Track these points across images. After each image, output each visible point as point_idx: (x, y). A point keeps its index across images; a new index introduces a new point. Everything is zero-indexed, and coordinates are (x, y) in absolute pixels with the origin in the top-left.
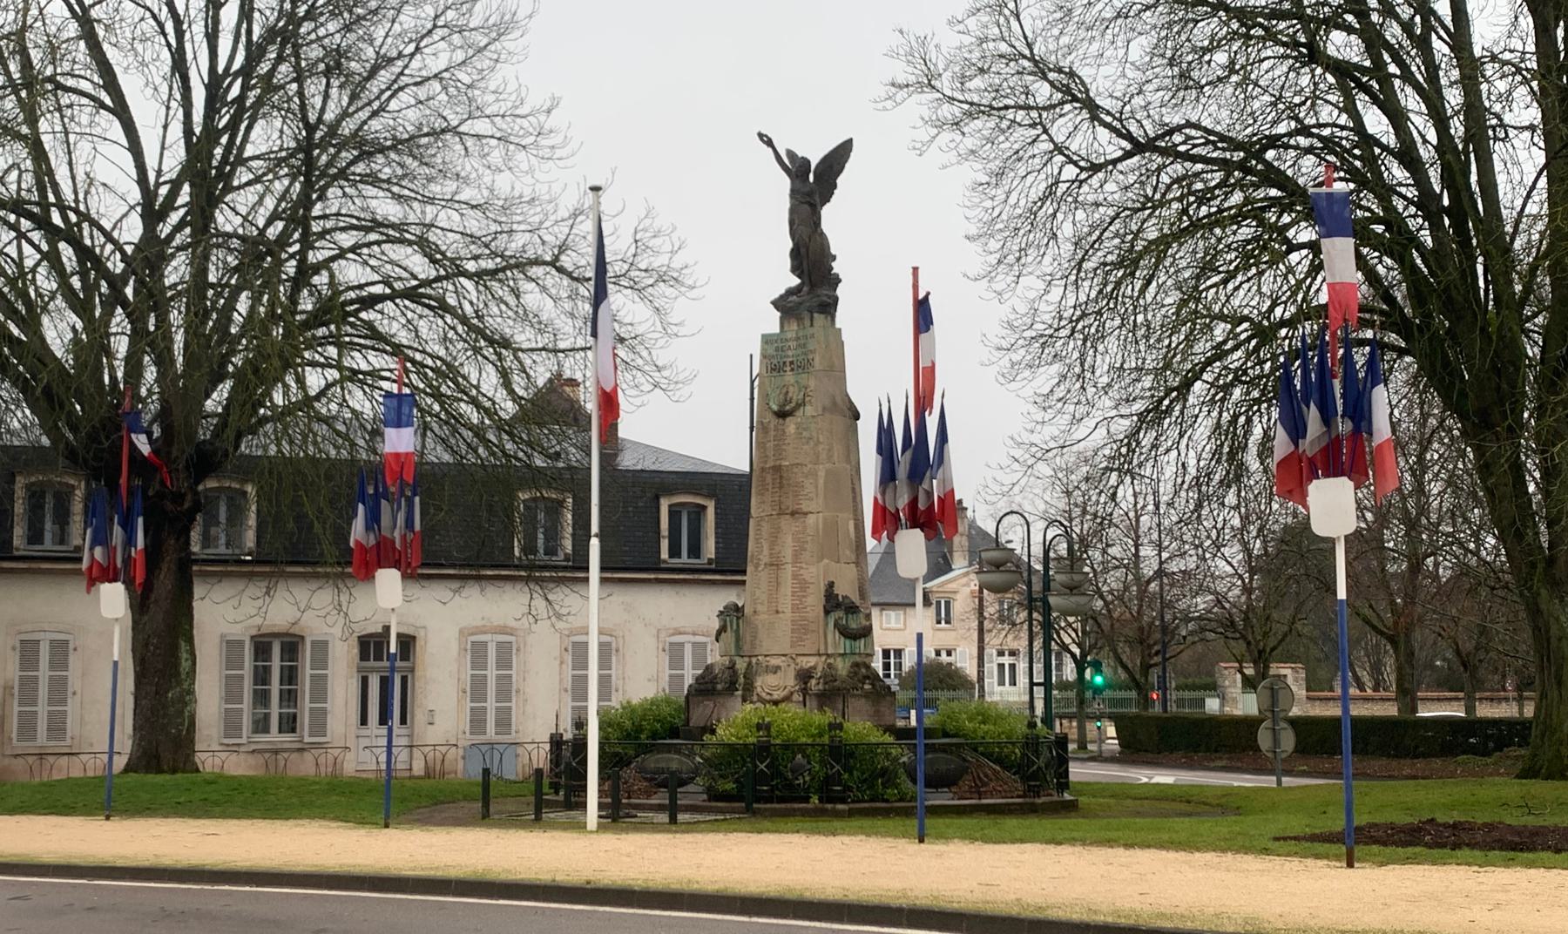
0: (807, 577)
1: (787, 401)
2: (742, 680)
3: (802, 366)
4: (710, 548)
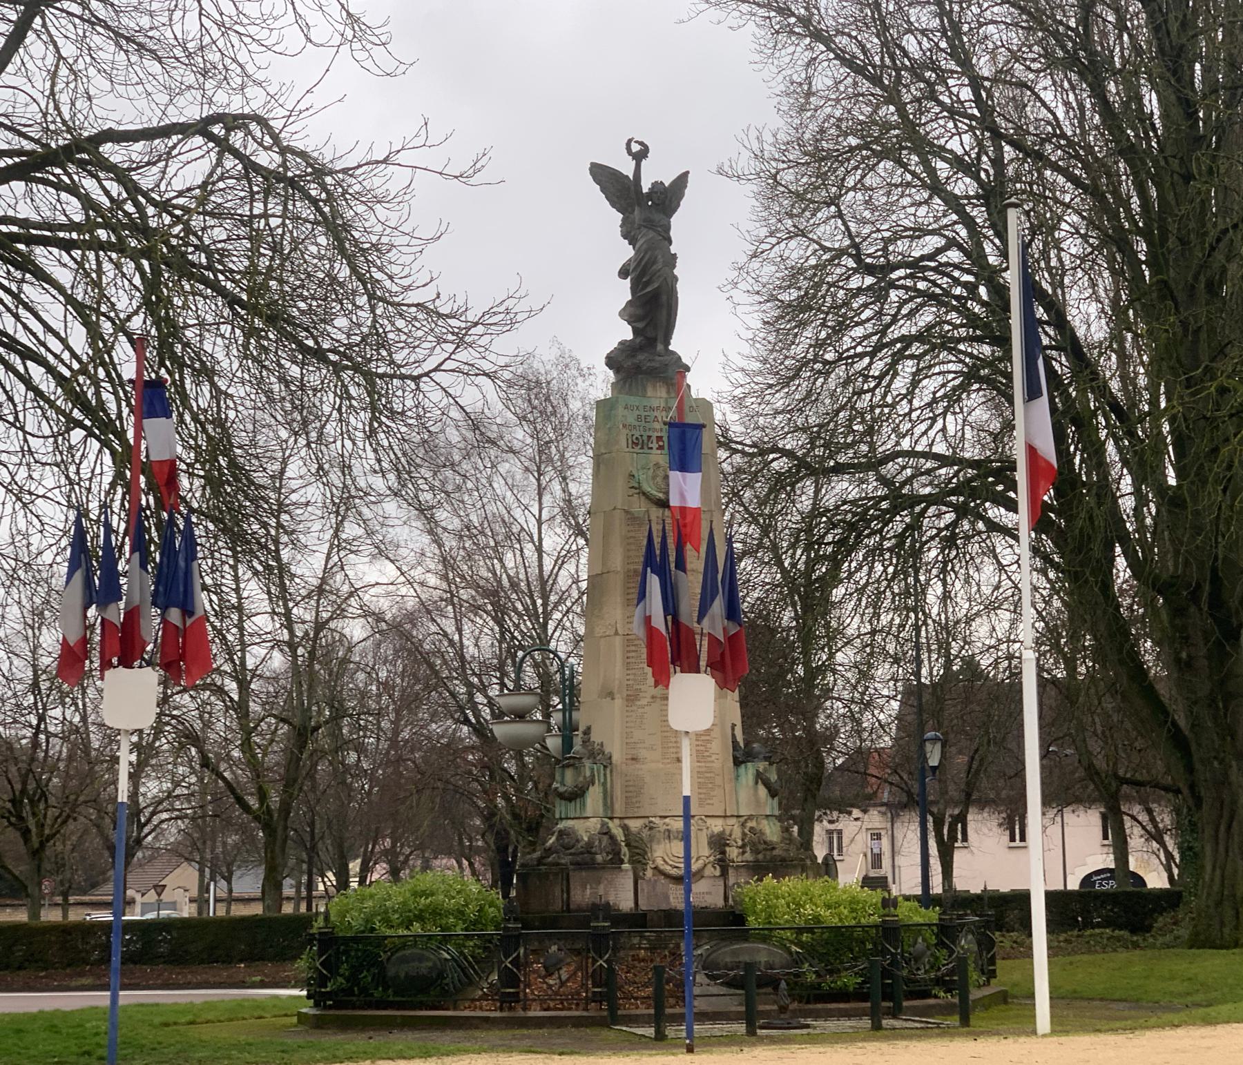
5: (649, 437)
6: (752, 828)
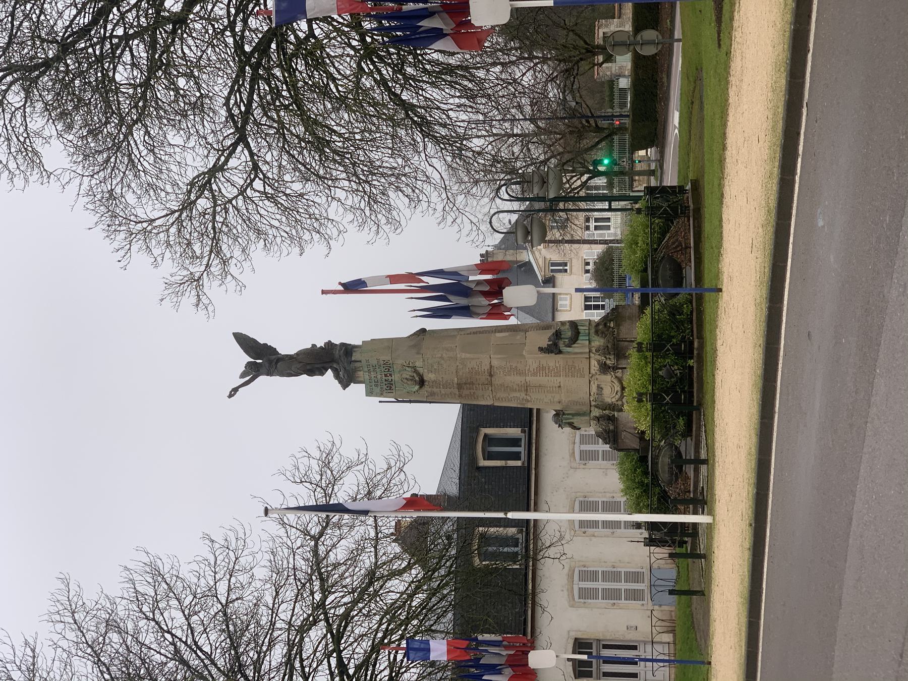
0: (535, 366)
1: (412, 379)
2: (607, 412)
3: (388, 368)
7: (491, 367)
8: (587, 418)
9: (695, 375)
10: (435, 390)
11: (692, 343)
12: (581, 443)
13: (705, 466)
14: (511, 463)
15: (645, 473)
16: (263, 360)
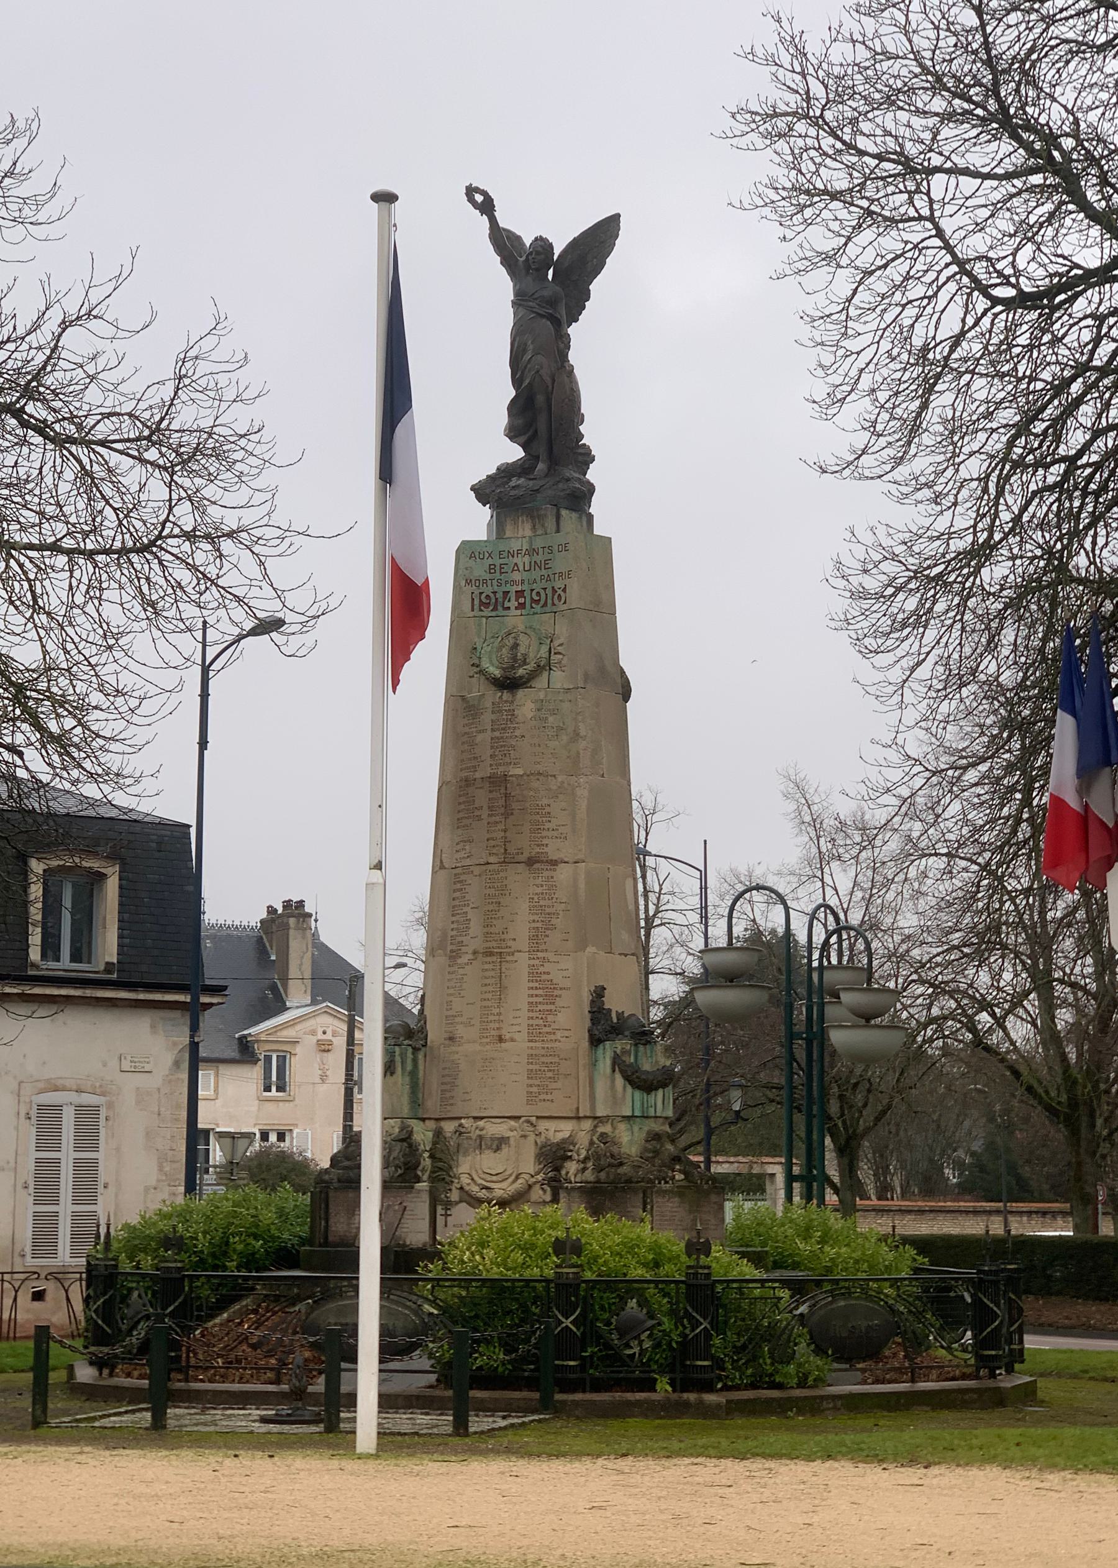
0: (557, 977)
1: (516, 661)
2: (426, 1162)
3: (544, 599)
4: (108, 945)
5: (506, 593)
6: (603, 1135)
7: (554, 863)
8: (406, 1111)
9: (629, 1396)
10: (487, 718)
11: (709, 1388)
12: (80, 1109)
13: (450, 1429)
14: (35, 938)
15: (250, 1261)
16: (552, 283)
